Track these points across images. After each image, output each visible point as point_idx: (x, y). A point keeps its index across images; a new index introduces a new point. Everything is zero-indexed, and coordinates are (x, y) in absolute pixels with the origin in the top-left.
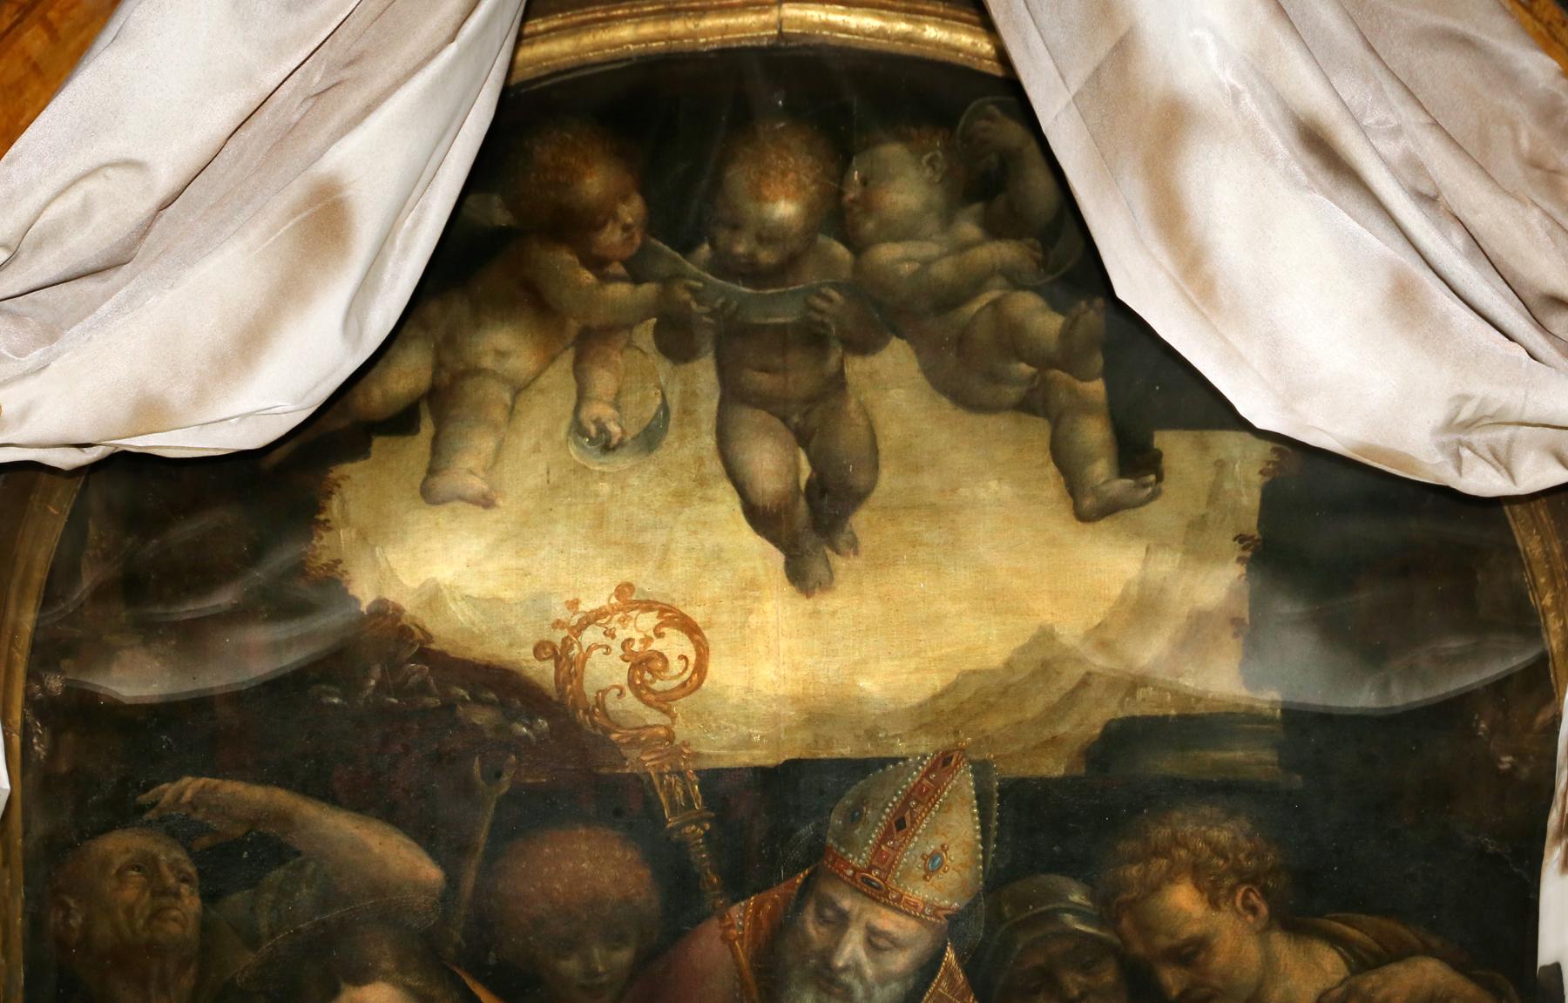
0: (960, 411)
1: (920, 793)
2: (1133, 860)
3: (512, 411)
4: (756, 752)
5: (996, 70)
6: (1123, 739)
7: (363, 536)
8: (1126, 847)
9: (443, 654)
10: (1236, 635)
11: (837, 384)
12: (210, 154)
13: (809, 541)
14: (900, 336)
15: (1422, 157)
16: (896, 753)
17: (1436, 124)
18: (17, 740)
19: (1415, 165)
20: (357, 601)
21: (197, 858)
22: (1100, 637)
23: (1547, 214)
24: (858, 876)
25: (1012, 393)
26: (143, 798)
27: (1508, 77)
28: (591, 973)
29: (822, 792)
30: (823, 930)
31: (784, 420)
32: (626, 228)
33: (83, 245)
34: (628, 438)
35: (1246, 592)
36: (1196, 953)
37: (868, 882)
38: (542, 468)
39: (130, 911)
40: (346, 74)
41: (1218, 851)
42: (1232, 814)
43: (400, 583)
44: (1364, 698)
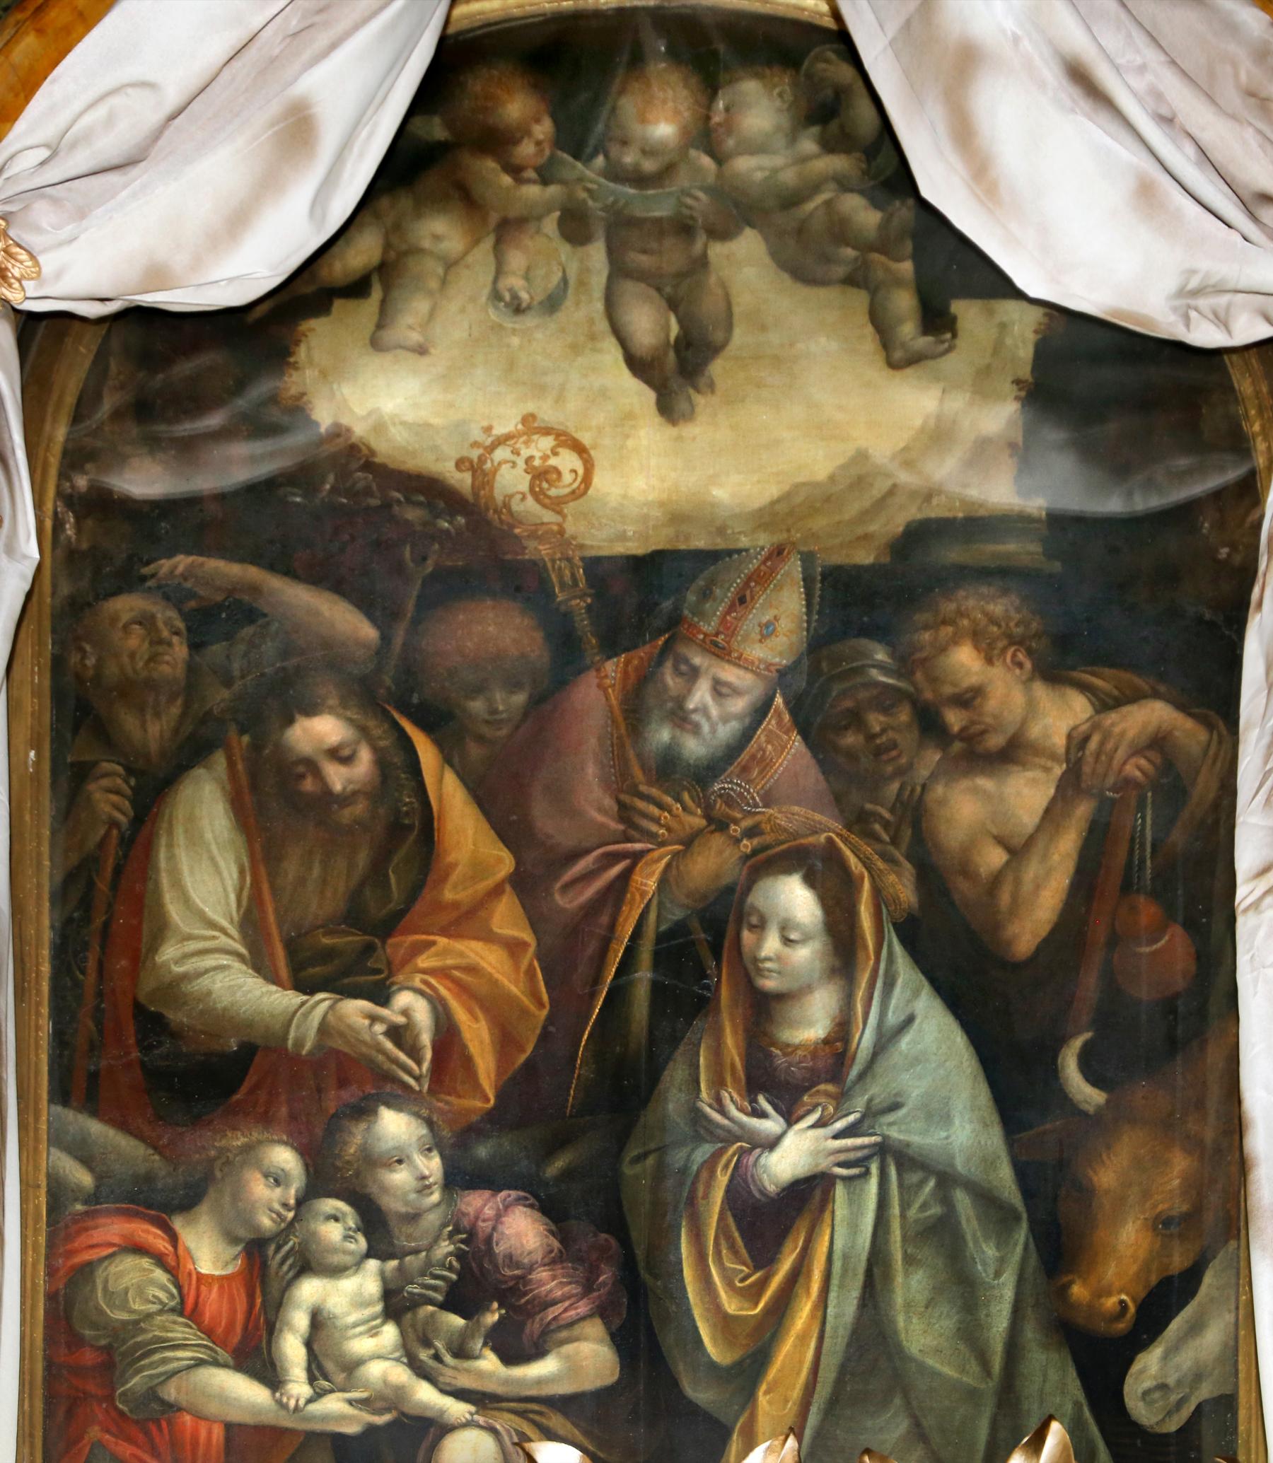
0: (799, 285)
1: (759, 576)
2: (926, 627)
3: (444, 282)
4: (630, 544)
5: (829, 23)
6: (921, 534)
7: (324, 374)
8: (921, 617)
9: (383, 467)
10: (1011, 456)
11: (702, 263)
12: (207, 77)
13: (675, 383)
14: (752, 226)
15: (1161, 88)
16: (740, 545)
17: (1173, 62)
18: (48, 524)
19: (1158, 96)
20: (317, 424)
21: (185, 616)
22: (907, 458)
23: (1260, 132)
24: (708, 641)
25: (840, 271)
26: (146, 571)
27: (1231, 28)
28: (494, 712)
29: (680, 575)
30: (678, 680)
31: (659, 290)
32: (538, 143)
33: (109, 146)
34: (535, 303)
35: (1020, 423)
36: (974, 698)
37: (715, 644)
38: (466, 325)
39: (132, 656)
40: (317, 19)
41: (993, 621)
42: (1005, 592)
43: (351, 411)
44: (1113, 504)
